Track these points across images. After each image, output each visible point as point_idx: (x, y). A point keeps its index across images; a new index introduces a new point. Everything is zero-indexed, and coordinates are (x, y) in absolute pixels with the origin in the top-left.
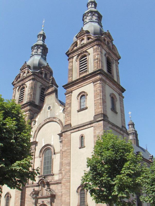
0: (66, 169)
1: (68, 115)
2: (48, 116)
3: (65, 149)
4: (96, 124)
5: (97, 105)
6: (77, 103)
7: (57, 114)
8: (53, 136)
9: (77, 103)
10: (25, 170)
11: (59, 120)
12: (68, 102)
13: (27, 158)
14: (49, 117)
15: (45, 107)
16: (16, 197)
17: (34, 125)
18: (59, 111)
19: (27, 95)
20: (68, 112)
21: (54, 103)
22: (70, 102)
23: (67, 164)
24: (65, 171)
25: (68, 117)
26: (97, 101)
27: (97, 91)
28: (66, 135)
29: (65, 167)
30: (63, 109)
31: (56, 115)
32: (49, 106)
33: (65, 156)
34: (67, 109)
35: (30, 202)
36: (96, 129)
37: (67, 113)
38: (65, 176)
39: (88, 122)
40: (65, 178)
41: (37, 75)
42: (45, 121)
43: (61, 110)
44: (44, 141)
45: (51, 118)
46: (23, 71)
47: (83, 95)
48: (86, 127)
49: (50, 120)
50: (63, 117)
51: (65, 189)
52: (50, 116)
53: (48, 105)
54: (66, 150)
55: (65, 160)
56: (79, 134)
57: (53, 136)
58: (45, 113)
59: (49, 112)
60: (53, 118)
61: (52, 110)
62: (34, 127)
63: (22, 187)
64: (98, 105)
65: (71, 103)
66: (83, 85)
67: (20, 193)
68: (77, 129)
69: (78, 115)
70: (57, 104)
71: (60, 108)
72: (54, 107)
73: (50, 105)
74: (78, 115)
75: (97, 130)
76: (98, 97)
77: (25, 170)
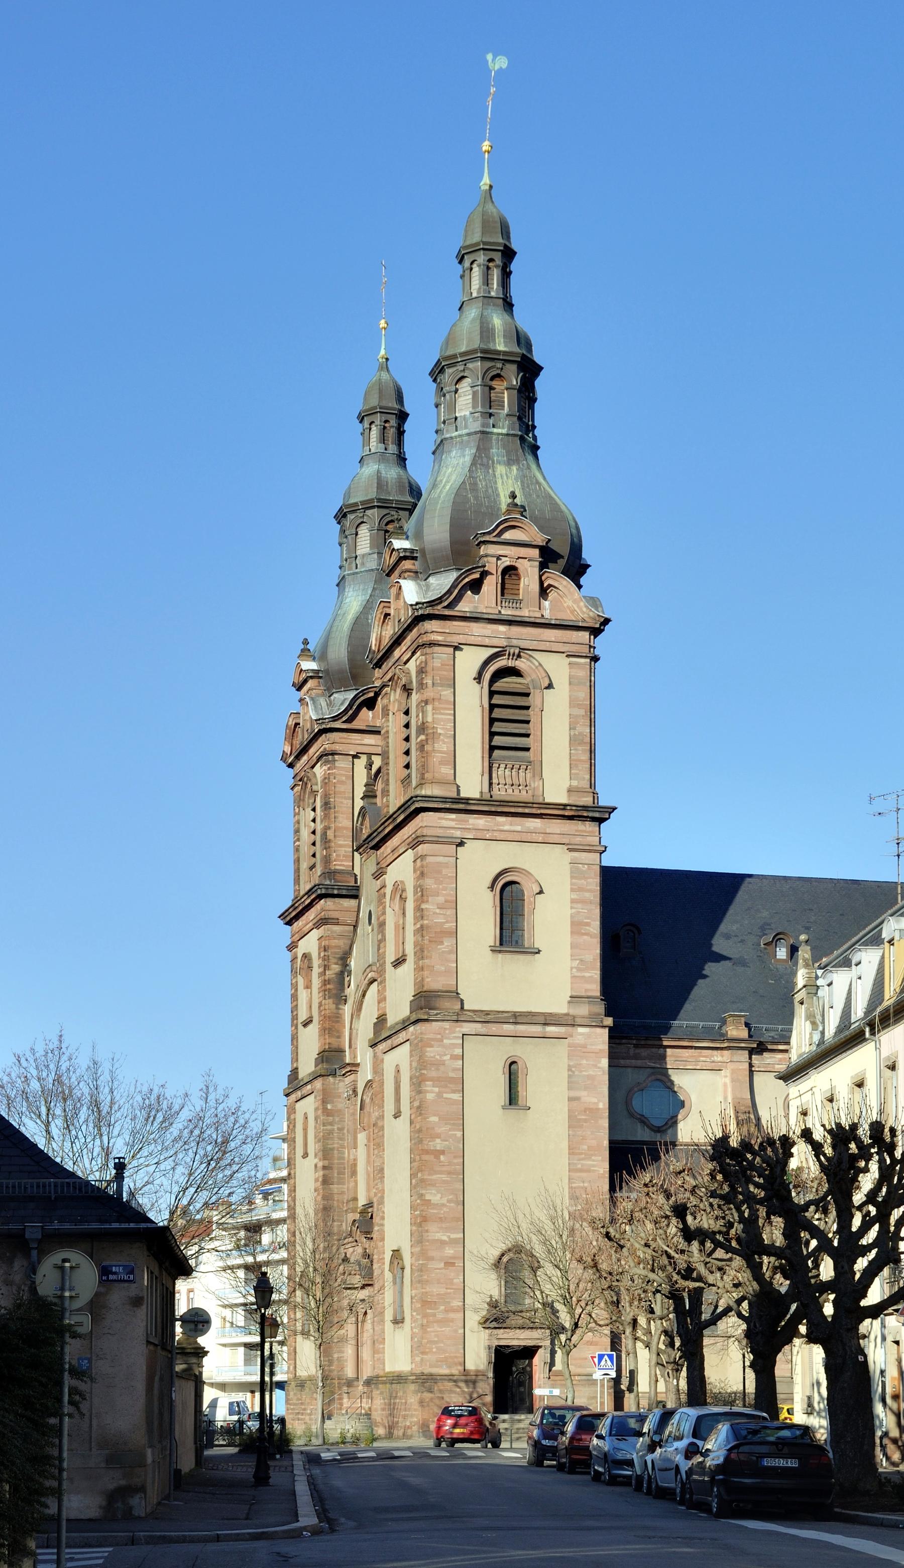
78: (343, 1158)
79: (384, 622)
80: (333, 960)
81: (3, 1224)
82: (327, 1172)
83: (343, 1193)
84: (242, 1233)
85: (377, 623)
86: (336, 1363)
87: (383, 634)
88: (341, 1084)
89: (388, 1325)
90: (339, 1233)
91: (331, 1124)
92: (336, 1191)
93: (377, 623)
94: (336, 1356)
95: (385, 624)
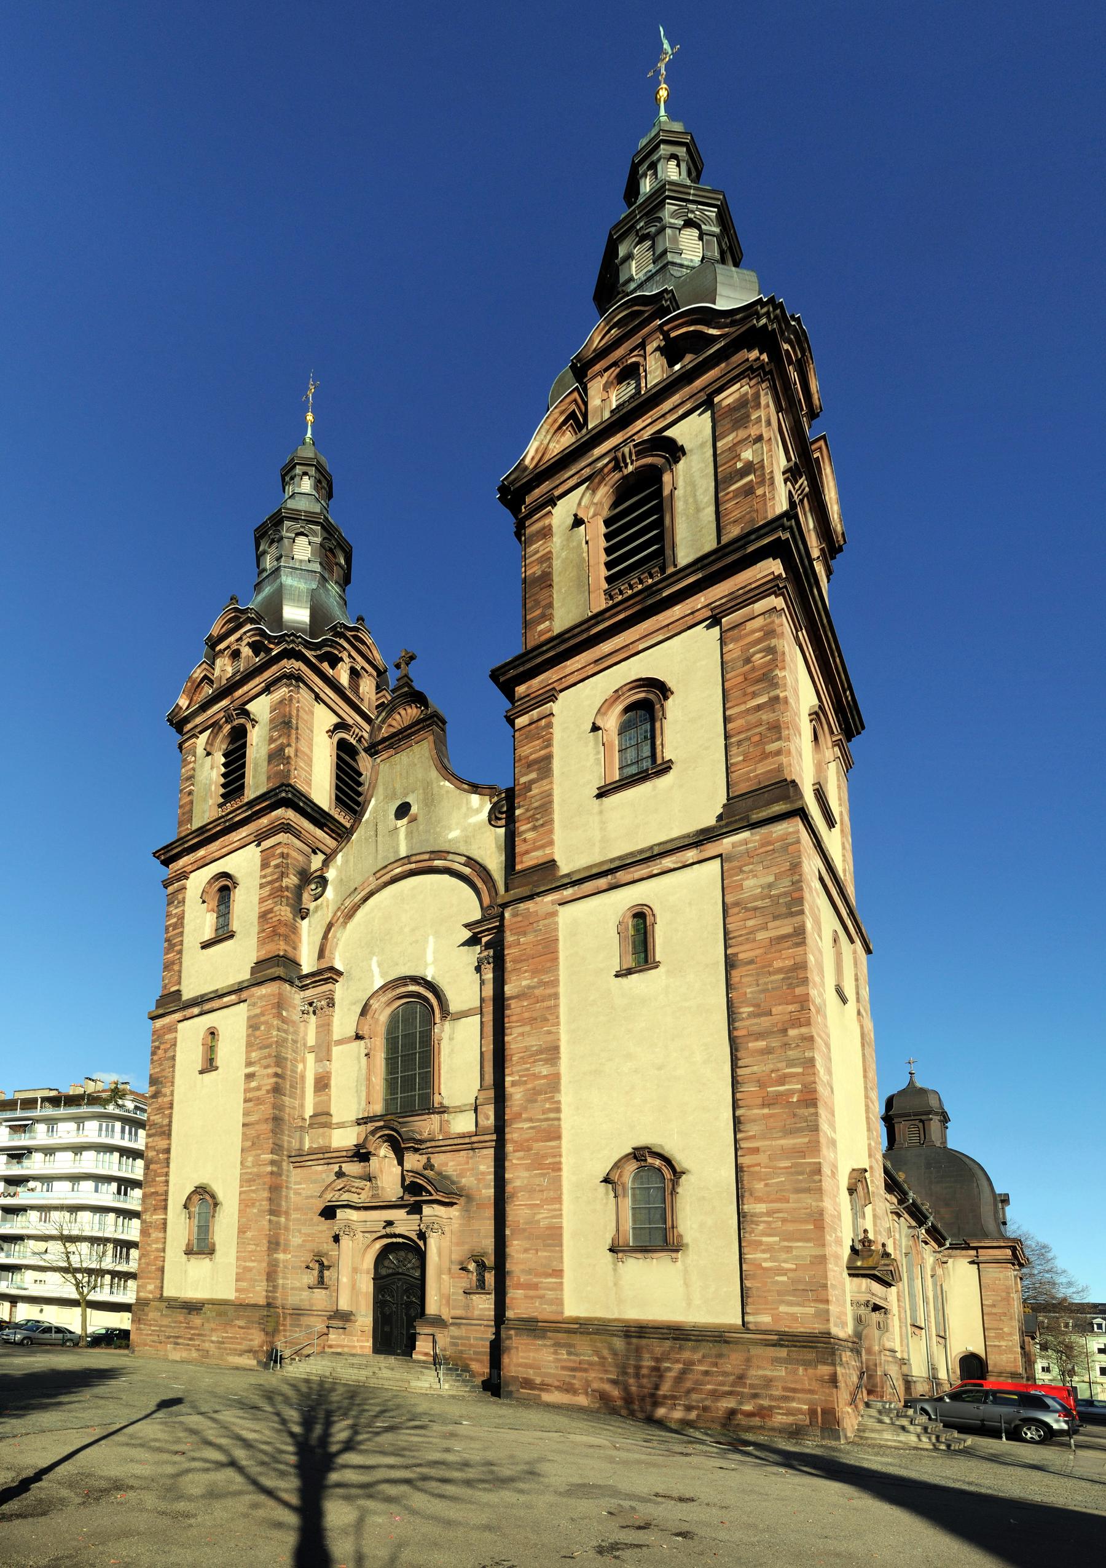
0: (536, 1076)
1: (537, 820)
2: (397, 852)
3: (524, 983)
4: (746, 842)
5: (748, 739)
6: (598, 753)
7: (453, 835)
8: (431, 939)
9: (598, 753)
10: (793, 323)
11: (471, 861)
12: (533, 757)
13: (165, 1096)
14: (403, 854)
15: (375, 811)
16: (245, 1204)
17: (316, 900)
18: (466, 816)
19: (266, 763)
20: (536, 805)
21: (428, 785)
22: (543, 753)
23: (540, 1052)
24: (529, 1086)
25: (534, 828)
26: (752, 718)
27: (748, 661)
28: (528, 914)
29: (528, 1069)
30: (489, 806)
31: (450, 841)
32: (398, 803)
33: (526, 1015)
34: (530, 790)
35: (320, 1228)
36: (746, 869)
37: (527, 810)
38: (526, 1109)
39: (688, 836)
40: (531, 1120)
41: (314, 660)
42: (378, 875)
43: (478, 811)
44: (379, 965)
45: (414, 859)
46: (228, 647)
47: (647, 704)
48: (668, 862)
49: (413, 866)
50: (494, 846)
51: (527, 1169)
52: (410, 846)
53: (394, 796)
54: (529, 987)
55: (522, 1034)
56: (616, 904)
57: (431, 939)
58: (380, 838)
59: (403, 829)
60: (426, 857)
61: (420, 819)
62: (317, 908)
63: (672, 115)
64: (757, 738)
65: (549, 758)
66: (641, 647)
67: (264, 1189)
68: (602, 882)
69: (601, 812)
70: (447, 784)
71: (468, 802)
72: (430, 801)
73: (406, 795)
74: (601, 812)
75: (751, 871)
76: (754, 695)
77: (793, 323)
78: (296, 1072)
79: (560, 428)
80: (291, 871)
81: (4, 1195)
82: (280, 1081)
83: (294, 1108)
84: (619, 1343)
85: (546, 427)
86: (280, 1290)
87: (551, 446)
88: (297, 996)
89: (228, 1194)
90: (288, 1150)
91: (286, 1032)
92: (287, 1104)
93: (546, 427)
94: (280, 1282)
95: (559, 434)
